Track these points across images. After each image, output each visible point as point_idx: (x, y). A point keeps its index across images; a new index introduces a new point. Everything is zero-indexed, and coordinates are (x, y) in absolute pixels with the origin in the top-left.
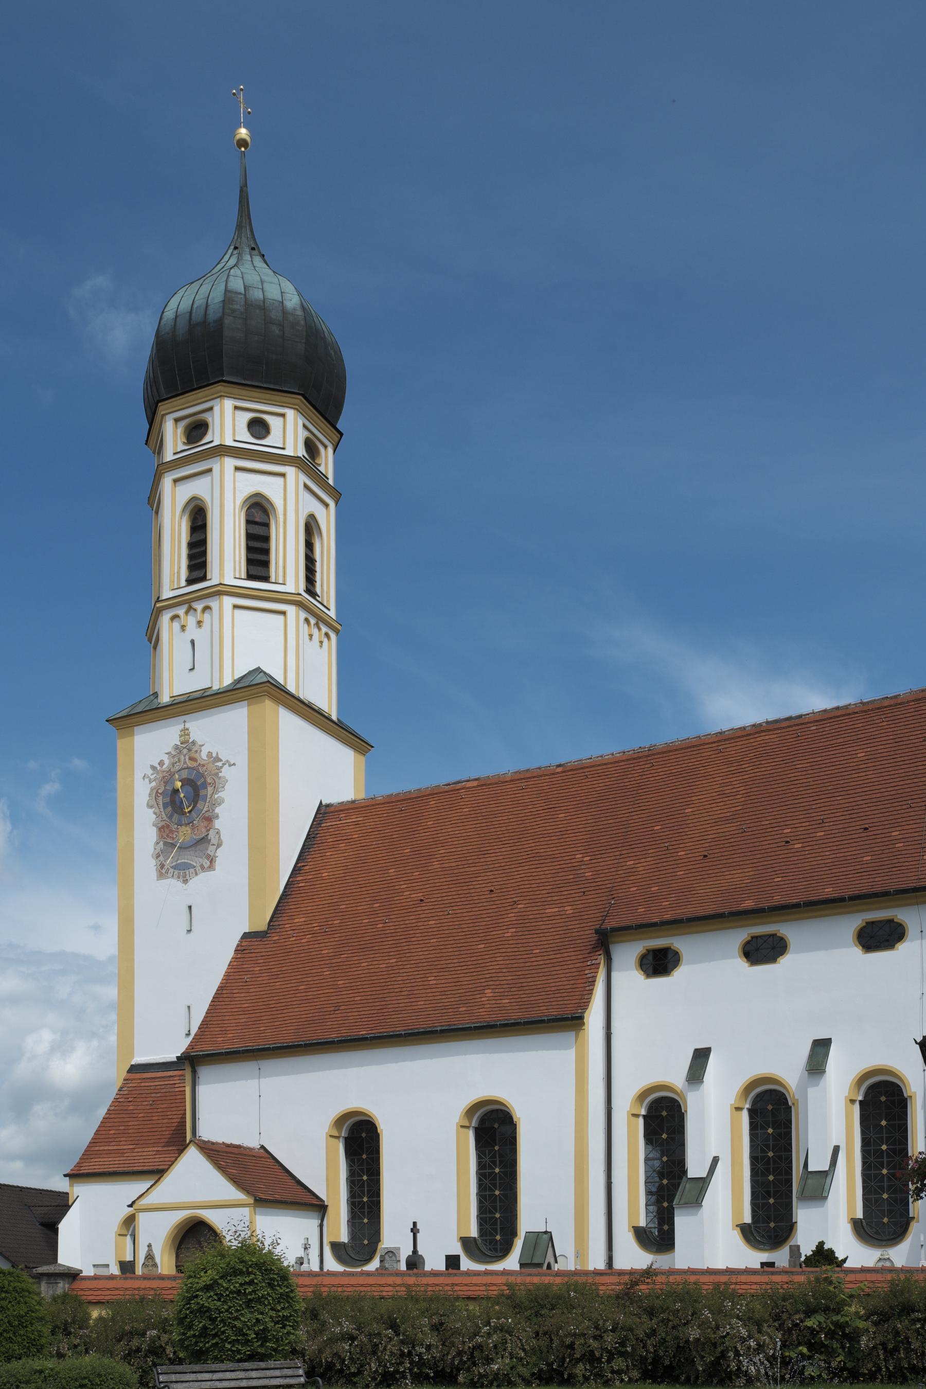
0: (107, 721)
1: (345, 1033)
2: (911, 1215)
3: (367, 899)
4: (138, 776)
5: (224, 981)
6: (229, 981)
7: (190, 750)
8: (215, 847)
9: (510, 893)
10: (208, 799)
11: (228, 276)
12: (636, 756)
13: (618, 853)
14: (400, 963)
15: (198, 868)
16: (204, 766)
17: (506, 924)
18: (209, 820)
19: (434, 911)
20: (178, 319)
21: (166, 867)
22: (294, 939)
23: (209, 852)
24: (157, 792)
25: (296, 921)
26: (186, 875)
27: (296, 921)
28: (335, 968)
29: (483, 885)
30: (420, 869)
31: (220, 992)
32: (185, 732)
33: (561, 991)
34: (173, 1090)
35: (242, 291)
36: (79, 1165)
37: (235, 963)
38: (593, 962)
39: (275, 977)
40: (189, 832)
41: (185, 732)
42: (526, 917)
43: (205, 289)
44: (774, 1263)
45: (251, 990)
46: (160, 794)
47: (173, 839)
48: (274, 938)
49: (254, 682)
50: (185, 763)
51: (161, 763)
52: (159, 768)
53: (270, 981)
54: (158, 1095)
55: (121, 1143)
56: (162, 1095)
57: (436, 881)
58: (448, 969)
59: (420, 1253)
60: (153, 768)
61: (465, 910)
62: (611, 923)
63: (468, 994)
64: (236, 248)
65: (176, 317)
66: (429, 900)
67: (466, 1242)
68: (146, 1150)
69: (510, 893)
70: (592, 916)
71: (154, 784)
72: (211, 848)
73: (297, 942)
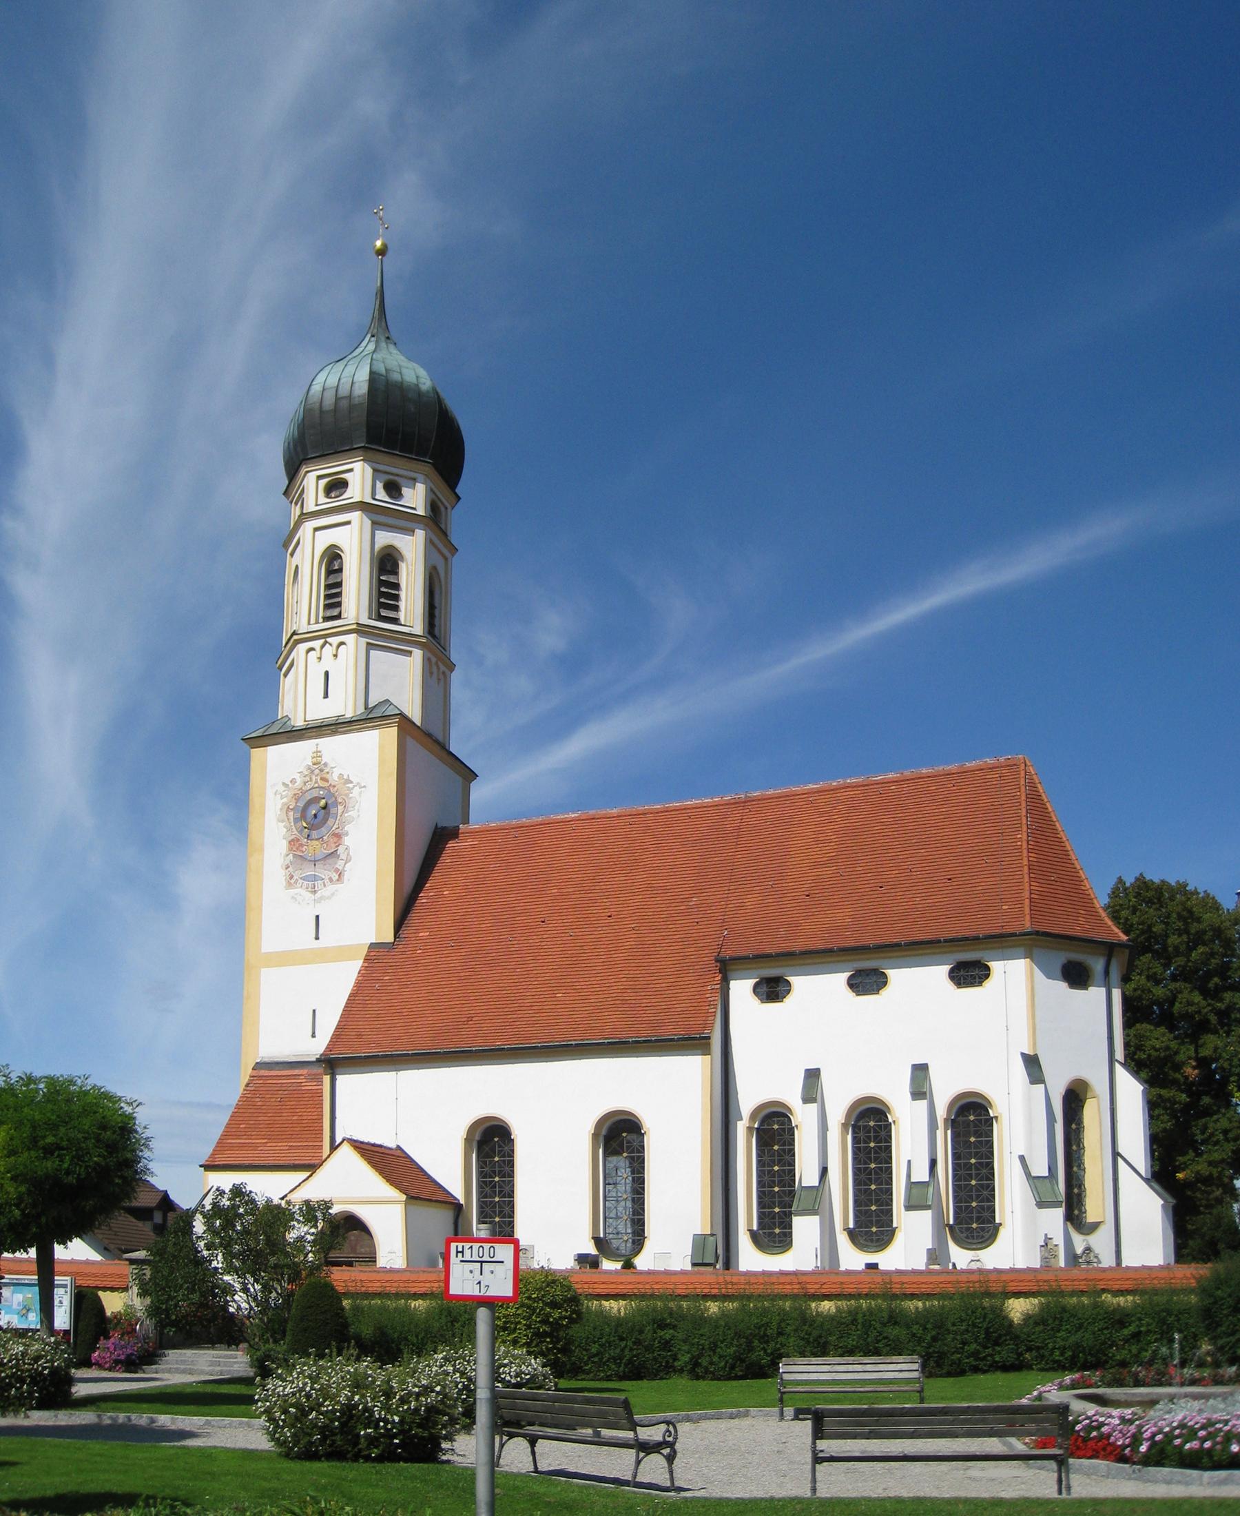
0: (243, 739)
2: (997, 1221)
4: (270, 793)
7: (321, 771)
8: (344, 862)
10: (338, 818)
11: (372, 359)
12: (733, 801)
13: (726, 888)
15: (327, 881)
16: (334, 786)
18: (338, 836)
20: (325, 393)
21: (295, 878)
23: (338, 866)
24: (288, 807)
25: (421, 935)
27: (421, 935)
32: (318, 754)
41: (318, 754)
43: (350, 369)
44: (877, 1264)
47: (303, 852)
49: (384, 714)
50: (316, 782)
51: (293, 781)
52: (290, 785)
54: (286, 1092)
55: (253, 1137)
56: (290, 1092)
62: (728, 953)
64: (373, 336)
65: (324, 390)
68: (280, 1144)
71: (285, 800)
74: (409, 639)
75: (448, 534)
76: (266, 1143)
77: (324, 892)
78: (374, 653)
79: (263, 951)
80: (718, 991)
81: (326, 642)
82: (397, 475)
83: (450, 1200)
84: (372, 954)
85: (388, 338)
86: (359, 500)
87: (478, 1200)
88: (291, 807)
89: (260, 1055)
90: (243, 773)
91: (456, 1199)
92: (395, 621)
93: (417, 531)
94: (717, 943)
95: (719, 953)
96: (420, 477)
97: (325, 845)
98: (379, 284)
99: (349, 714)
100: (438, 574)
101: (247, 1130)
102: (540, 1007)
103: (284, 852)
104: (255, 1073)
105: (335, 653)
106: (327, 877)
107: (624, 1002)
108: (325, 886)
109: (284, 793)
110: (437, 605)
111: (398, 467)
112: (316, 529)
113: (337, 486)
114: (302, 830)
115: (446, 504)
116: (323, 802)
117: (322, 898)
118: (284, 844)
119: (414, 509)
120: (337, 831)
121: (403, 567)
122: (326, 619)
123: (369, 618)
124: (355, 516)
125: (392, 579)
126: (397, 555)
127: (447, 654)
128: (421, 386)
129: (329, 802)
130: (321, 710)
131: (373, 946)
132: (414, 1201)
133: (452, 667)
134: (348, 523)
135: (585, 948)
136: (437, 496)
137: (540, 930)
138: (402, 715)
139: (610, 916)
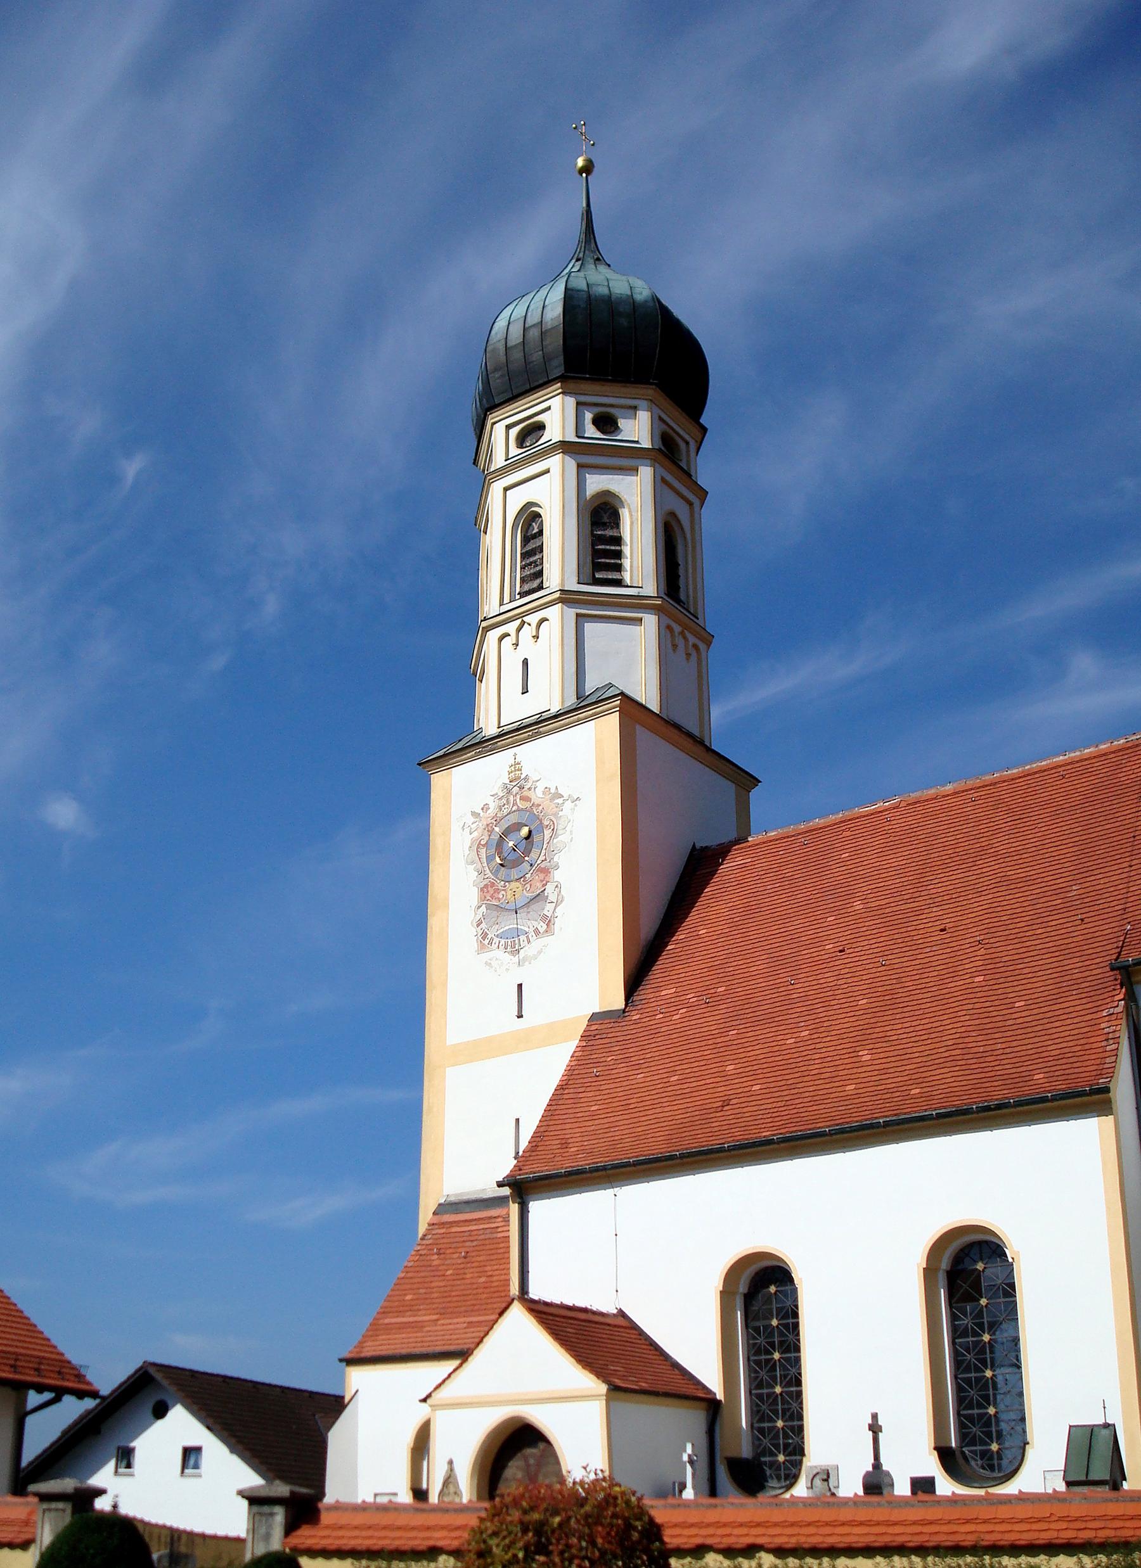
0: (419, 764)
1: (738, 1135)
3: (763, 957)
4: (455, 828)
5: (566, 1078)
6: (572, 1077)
7: (521, 788)
8: (554, 904)
9: (970, 931)
12: (1129, 745)
14: (815, 1036)
17: (969, 971)
19: (860, 963)
21: (489, 936)
22: (661, 1016)
24: (480, 843)
25: (663, 993)
26: (515, 944)
27: (663, 993)
28: (722, 1050)
29: (930, 925)
30: (835, 913)
31: (558, 1092)
32: (516, 766)
33: (1067, 1055)
34: (495, 1235)
35: (586, 289)
36: (361, 1344)
37: (581, 1053)
38: (1112, 1011)
39: (637, 1067)
40: (521, 888)
41: (516, 766)
42: (997, 960)
45: (603, 1088)
46: (483, 845)
47: (499, 900)
48: (634, 1018)
51: (485, 808)
52: (482, 814)
53: (628, 1074)
55: (420, 1313)
57: (860, 925)
58: (887, 1039)
59: (885, 1468)
60: (474, 814)
61: (906, 959)
63: (921, 1070)
64: (578, 260)
66: (852, 950)
67: (946, 1456)
69: (970, 931)
70: (1100, 949)
71: (475, 834)
72: (548, 909)
73: (667, 1019)
74: (638, 603)
75: (693, 473)
76: (438, 1320)
77: (527, 951)
78: (589, 627)
79: (448, 1043)
80: (1120, 1016)
81: (523, 623)
82: (612, 406)
83: (691, 1390)
84: (594, 1028)
85: (598, 259)
86: (558, 440)
87: (750, 1393)
88: (482, 843)
89: (445, 1193)
90: (421, 803)
91: (709, 1391)
92: (619, 583)
93: (641, 469)
94: (1115, 945)
95: (1119, 953)
96: (643, 404)
97: (528, 885)
98: (584, 205)
99: (554, 710)
100: (678, 521)
101: (413, 1303)
102: (834, 1074)
103: (475, 902)
104: (436, 1219)
105: (534, 634)
106: (532, 929)
107: (965, 1051)
108: (529, 942)
109: (472, 826)
110: (681, 560)
111: (608, 396)
112: (506, 489)
113: (532, 430)
114: (497, 871)
115: (687, 437)
116: (525, 831)
117: (525, 959)
118: (474, 895)
119: (637, 442)
120: (542, 865)
121: (625, 514)
122: (523, 594)
123: (578, 583)
124: (555, 462)
125: (609, 533)
126: (616, 503)
127: (700, 622)
128: (635, 296)
129: (532, 828)
130: (518, 709)
131: (594, 1017)
132: (622, 1395)
133: (708, 639)
134: (547, 471)
135: (904, 980)
136: (667, 424)
137: (837, 963)
138: (622, 694)
139: (942, 930)
